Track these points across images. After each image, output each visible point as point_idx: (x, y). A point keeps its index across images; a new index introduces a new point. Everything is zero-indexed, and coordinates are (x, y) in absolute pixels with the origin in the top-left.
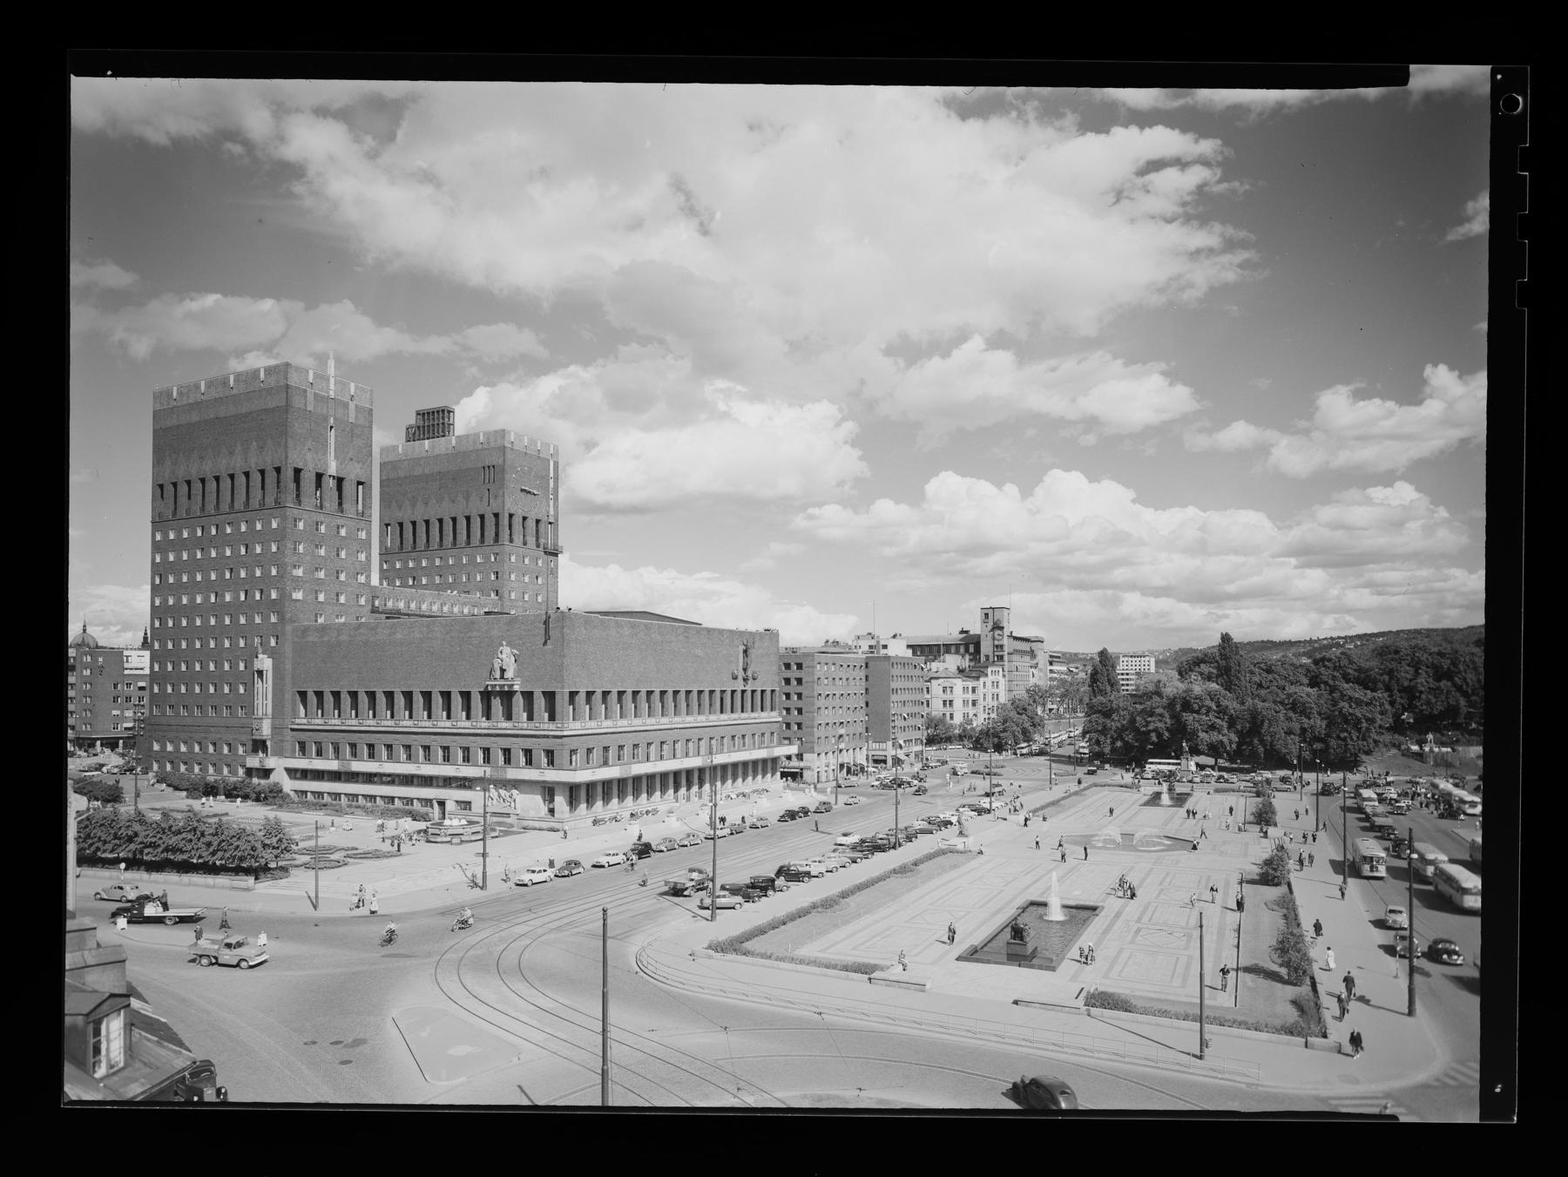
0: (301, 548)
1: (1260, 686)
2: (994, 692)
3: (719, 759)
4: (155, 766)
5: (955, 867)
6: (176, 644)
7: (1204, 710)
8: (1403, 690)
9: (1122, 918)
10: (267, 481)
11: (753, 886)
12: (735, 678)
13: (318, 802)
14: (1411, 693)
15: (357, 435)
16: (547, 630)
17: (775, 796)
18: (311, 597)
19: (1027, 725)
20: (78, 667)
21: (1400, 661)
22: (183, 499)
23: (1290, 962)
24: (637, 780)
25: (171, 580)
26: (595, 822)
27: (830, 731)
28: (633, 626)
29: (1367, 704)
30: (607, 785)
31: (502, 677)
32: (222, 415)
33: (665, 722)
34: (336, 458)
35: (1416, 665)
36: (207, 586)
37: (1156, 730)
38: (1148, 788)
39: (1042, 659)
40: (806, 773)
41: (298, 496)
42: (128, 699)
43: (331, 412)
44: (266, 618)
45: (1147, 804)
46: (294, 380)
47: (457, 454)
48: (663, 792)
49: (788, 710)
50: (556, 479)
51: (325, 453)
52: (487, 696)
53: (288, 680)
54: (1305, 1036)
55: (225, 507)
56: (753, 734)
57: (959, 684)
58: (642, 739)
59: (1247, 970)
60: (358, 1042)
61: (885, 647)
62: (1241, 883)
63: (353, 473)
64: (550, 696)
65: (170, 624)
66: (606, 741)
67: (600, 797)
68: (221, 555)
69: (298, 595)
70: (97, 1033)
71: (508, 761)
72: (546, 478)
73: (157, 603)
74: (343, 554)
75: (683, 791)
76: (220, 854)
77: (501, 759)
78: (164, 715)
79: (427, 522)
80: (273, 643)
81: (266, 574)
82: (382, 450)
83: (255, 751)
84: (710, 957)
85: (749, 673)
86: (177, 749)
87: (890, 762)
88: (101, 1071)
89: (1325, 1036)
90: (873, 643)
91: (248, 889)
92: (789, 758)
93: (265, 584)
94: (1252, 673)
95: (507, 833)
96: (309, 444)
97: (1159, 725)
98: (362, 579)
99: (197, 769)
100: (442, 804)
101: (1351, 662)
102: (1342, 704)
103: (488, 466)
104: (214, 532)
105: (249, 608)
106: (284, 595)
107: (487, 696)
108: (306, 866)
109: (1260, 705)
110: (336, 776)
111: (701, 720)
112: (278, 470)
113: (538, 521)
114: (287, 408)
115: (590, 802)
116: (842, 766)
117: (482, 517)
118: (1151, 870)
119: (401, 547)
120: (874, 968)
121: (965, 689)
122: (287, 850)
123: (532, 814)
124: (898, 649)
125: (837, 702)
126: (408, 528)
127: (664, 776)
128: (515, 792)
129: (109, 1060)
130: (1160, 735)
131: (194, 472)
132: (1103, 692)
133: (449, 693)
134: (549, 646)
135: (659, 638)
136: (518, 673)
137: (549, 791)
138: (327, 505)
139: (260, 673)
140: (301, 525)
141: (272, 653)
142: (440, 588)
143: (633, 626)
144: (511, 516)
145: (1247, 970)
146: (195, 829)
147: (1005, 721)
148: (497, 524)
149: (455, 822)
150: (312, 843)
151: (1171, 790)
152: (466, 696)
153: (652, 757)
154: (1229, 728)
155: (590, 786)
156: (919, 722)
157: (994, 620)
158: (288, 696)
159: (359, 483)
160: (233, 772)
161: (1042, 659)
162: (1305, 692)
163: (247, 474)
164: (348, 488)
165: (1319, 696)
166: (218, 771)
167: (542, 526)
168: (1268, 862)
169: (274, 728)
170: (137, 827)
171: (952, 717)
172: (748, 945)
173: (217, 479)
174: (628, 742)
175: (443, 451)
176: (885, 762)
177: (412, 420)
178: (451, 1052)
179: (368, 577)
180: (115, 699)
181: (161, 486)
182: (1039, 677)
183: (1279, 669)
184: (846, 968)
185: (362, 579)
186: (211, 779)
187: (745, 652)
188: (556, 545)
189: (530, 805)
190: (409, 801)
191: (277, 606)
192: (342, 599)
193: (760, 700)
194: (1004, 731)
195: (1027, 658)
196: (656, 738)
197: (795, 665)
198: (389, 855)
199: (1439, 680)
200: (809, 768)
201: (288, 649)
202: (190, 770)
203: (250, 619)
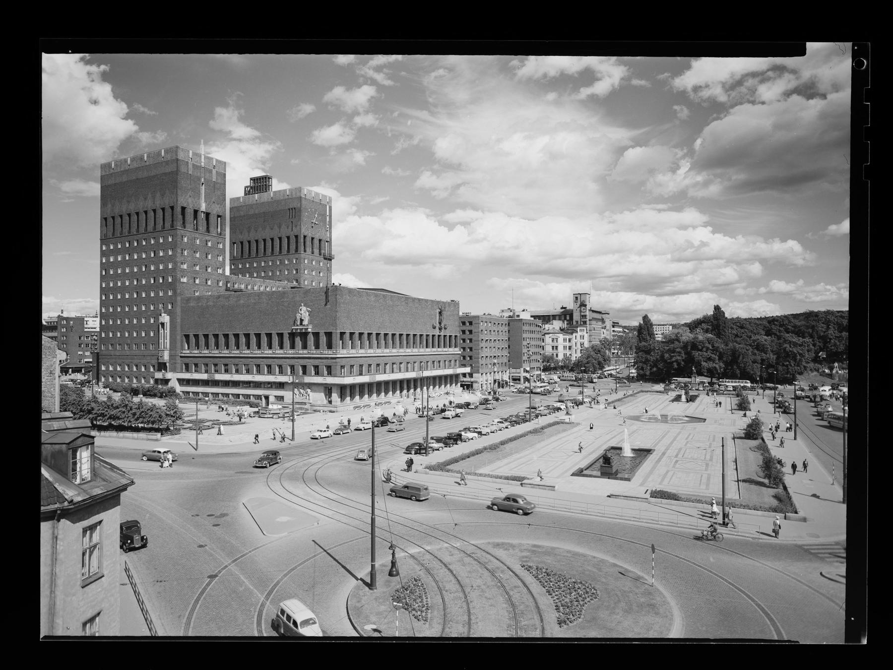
0: (185, 253)
1: (737, 336)
2: (582, 339)
3: (427, 374)
4: (103, 379)
5: (564, 431)
6: (115, 309)
7: (704, 349)
8: (820, 337)
9: (666, 455)
10: (166, 214)
11: (449, 438)
12: (434, 328)
13: (196, 398)
14: (825, 339)
15: (218, 186)
16: (327, 297)
17: (459, 395)
18: (191, 281)
19: (601, 360)
20: (59, 327)
21: (818, 321)
22: (118, 226)
23: (771, 471)
24: (379, 384)
25: (112, 272)
26: (355, 408)
27: (488, 361)
28: (376, 296)
29: (800, 345)
30: (362, 386)
31: (301, 324)
32: (140, 177)
33: (394, 352)
34: (206, 201)
35: (827, 323)
36: (132, 276)
37: (677, 361)
38: (673, 394)
39: (608, 324)
40: (475, 385)
41: (184, 223)
42: (87, 345)
43: (203, 175)
44: (166, 293)
45: (673, 401)
46: (181, 156)
47: (275, 202)
48: (394, 392)
49: (464, 349)
50: (330, 216)
51: (199, 198)
52: (292, 335)
53: (179, 328)
54: (784, 513)
55: (142, 230)
56: (444, 360)
57: (561, 337)
58: (381, 361)
59: (744, 481)
60: (223, 515)
61: (518, 316)
62: (734, 438)
63: (215, 210)
64: (329, 335)
65: (111, 297)
66: (361, 361)
67: (358, 393)
68: (140, 257)
69: (185, 280)
70: (74, 457)
71: (304, 373)
72: (324, 215)
73: (104, 286)
74: (209, 257)
75: (405, 392)
76: (141, 419)
77: (301, 372)
78: (108, 349)
79: (257, 241)
80: (170, 307)
81: (166, 267)
82: (231, 200)
83: (159, 370)
84: (426, 473)
85: (443, 325)
86: (115, 369)
87: (522, 380)
88: (78, 481)
89: (796, 512)
90: (511, 314)
91: (157, 440)
92: (464, 375)
93: (165, 273)
94: (732, 328)
95: (304, 413)
96: (190, 193)
97: (679, 358)
98: (220, 271)
99: (127, 380)
100: (267, 398)
101: (790, 322)
102: (785, 345)
103: (291, 209)
104: (136, 244)
105: (156, 287)
106: (175, 280)
107: (292, 335)
108: (190, 428)
109: (737, 346)
110: (206, 383)
111: (415, 351)
113: (320, 240)
114: (177, 172)
115: (352, 397)
116: (495, 381)
117: (288, 238)
118: (680, 433)
119: (242, 256)
120: (524, 478)
121: (565, 340)
122: (180, 418)
123: (319, 403)
124: (526, 316)
125: (492, 344)
126: (246, 245)
127: (394, 382)
128: (309, 390)
129: (81, 476)
130: (679, 364)
131: (124, 210)
132: (645, 340)
133: (271, 334)
134: (328, 306)
135: (391, 303)
136: (310, 322)
137: (328, 390)
138: (200, 228)
139: (163, 324)
140: (185, 240)
141: (169, 313)
142: (266, 277)
143: (376, 296)
144: (305, 237)
145: (744, 481)
146: (126, 406)
147: (588, 357)
148: (297, 242)
149: (275, 407)
150: (194, 418)
151: (686, 393)
152: (280, 336)
153: (387, 371)
154: (719, 359)
155: (352, 387)
156: (539, 357)
157: (580, 300)
158: (179, 337)
159: (219, 216)
160: (148, 382)
161: (608, 324)
162: (764, 339)
163: (154, 211)
164: (212, 219)
165: (772, 341)
166: (139, 381)
167: (322, 242)
168: (750, 426)
169: (171, 356)
170: (93, 405)
171: (557, 355)
172: (449, 467)
173: (137, 214)
174: (374, 363)
175: (266, 200)
176: (519, 380)
177: (248, 183)
178: (278, 520)
179: (224, 270)
180: (80, 345)
181: (106, 219)
182: (607, 334)
183: (748, 326)
184: (507, 478)
185: (220, 271)
186: (135, 386)
187: (440, 313)
188: (330, 254)
189: (318, 398)
190: (248, 396)
191: (173, 286)
192: (209, 283)
193: (449, 341)
194: (588, 363)
195: (600, 323)
196: (390, 361)
197: (468, 323)
198: (235, 424)
199: (841, 332)
200: (476, 382)
201: (178, 310)
202: (123, 381)
203: (157, 294)
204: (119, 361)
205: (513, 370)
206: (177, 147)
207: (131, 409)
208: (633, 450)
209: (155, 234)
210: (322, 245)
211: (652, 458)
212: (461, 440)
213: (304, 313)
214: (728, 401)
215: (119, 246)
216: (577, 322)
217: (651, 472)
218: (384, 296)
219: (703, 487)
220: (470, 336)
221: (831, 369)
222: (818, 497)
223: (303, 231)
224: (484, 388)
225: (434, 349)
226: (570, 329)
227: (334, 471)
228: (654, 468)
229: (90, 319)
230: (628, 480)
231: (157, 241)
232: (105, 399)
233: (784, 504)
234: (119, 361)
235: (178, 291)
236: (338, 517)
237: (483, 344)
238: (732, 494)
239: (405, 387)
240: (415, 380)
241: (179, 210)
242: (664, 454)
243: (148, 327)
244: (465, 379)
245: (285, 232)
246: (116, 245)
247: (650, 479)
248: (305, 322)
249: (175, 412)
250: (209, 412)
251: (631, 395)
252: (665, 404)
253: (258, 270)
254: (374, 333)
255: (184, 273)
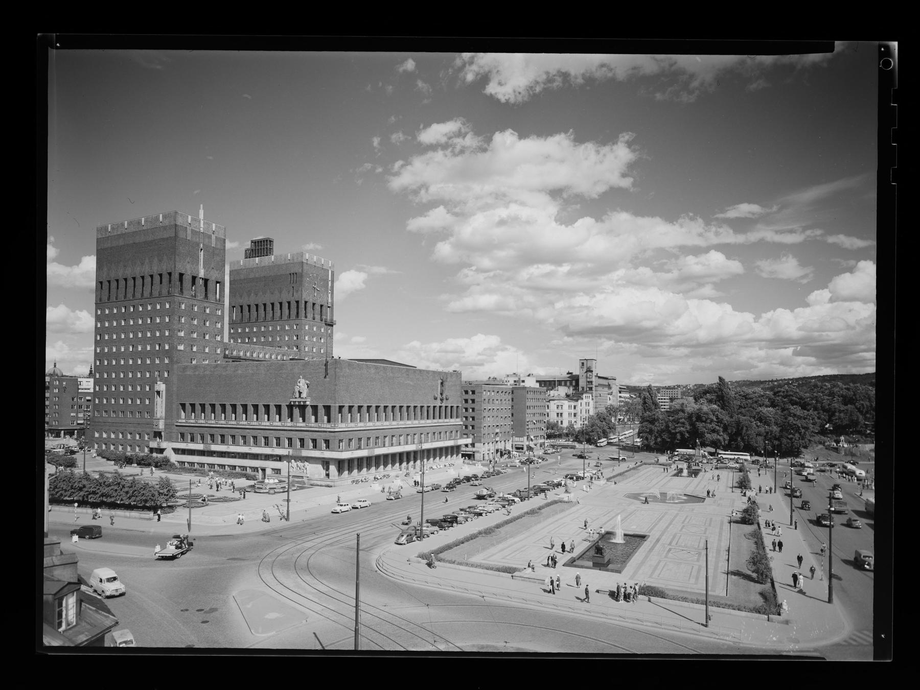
0: (183, 320)
2: (587, 407)
3: (426, 446)
4: (96, 446)
5: (562, 511)
8: (824, 410)
11: (445, 521)
12: (436, 399)
15: (217, 255)
16: (326, 370)
18: (189, 349)
20: (51, 388)
23: (758, 571)
24: (378, 457)
27: (491, 430)
28: (376, 368)
32: (137, 241)
34: (204, 267)
36: (127, 342)
37: (681, 433)
39: (615, 389)
40: (476, 455)
41: (181, 289)
43: (201, 240)
44: (162, 360)
46: (180, 221)
49: (466, 418)
52: (290, 407)
57: (566, 403)
58: (381, 434)
60: (213, 610)
61: (523, 381)
62: (730, 523)
63: (214, 276)
69: (181, 347)
70: (60, 605)
71: (302, 446)
72: (326, 281)
76: (133, 498)
78: (102, 416)
80: (166, 375)
81: (162, 335)
85: (444, 396)
86: (109, 436)
87: (525, 448)
88: (64, 627)
90: (516, 379)
91: (150, 519)
92: (467, 446)
95: (302, 488)
98: (219, 338)
99: (120, 448)
100: (264, 470)
103: (294, 275)
104: (132, 309)
105: (152, 354)
106: (173, 348)
107: (290, 407)
109: (742, 418)
112: (170, 274)
113: (321, 306)
116: (497, 451)
118: (677, 514)
121: (570, 407)
123: (316, 477)
124: (531, 383)
125: (495, 413)
132: (650, 410)
134: (327, 379)
136: (309, 395)
137: (326, 463)
139: (158, 393)
140: (183, 307)
141: (165, 381)
143: (376, 368)
144: (306, 302)
147: (593, 426)
149: (271, 481)
150: (187, 492)
151: (689, 467)
153: (387, 444)
155: (350, 461)
156: (543, 426)
160: (142, 450)
161: (615, 389)
162: (768, 411)
164: (211, 285)
166: (133, 449)
167: (324, 308)
169: (166, 425)
174: (373, 436)
175: (267, 264)
176: (522, 449)
179: (222, 337)
181: (101, 283)
182: (614, 399)
185: (219, 338)
186: (129, 454)
187: (442, 383)
188: (332, 319)
189: (316, 471)
190: (244, 468)
193: (450, 412)
195: (606, 389)
197: (471, 392)
200: (478, 452)
204: (113, 429)
205: (517, 439)
206: (176, 212)
207: (123, 487)
208: (625, 535)
209: (152, 300)
210: (324, 311)
211: (646, 545)
212: (457, 522)
213: (302, 384)
214: (729, 477)
215: (115, 311)
216: (583, 388)
217: (643, 563)
218: (384, 368)
219: (693, 581)
220: (473, 406)
221: (838, 442)
222: (804, 594)
223: (304, 296)
224: (487, 458)
225: (435, 421)
226: (575, 396)
227: (326, 560)
228: (646, 557)
229: (84, 380)
230: (619, 572)
231: (154, 308)
232: (97, 477)
233: (770, 604)
234: (113, 429)
235: (175, 359)
236: (327, 613)
237: (486, 414)
238: (719, 590)
239: (405, 459)
240: (415, 452)
241: (177, 276)
242: (658, 540)
243: (143, 396)
244: (467, 449)
245: (285, 297)
246: (111, 310)
247: (641, 572)
248: (304, 395)
249: (169, 491)
250: (202, 486)
251: (634, 468)
252: (665, 481)
253: (259, 334)
254: (374, 405)
255: (181, 340)
